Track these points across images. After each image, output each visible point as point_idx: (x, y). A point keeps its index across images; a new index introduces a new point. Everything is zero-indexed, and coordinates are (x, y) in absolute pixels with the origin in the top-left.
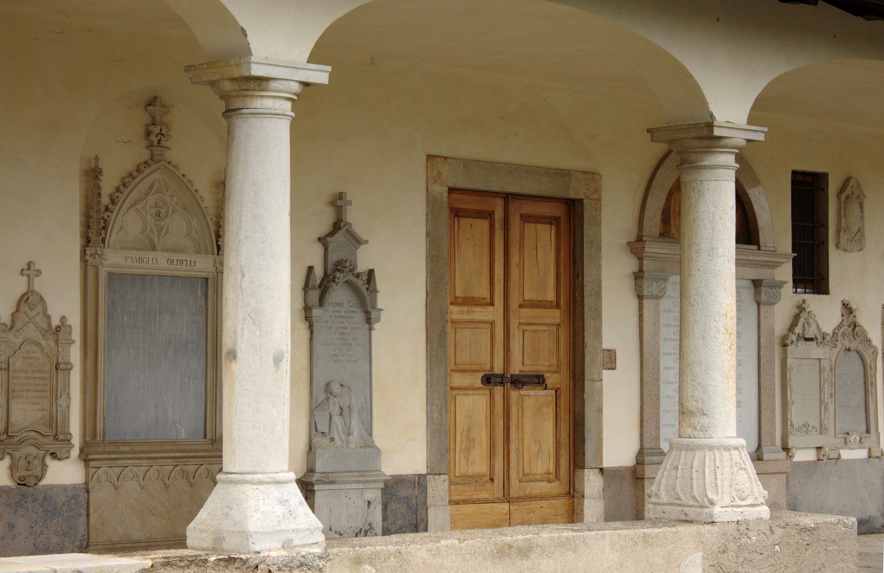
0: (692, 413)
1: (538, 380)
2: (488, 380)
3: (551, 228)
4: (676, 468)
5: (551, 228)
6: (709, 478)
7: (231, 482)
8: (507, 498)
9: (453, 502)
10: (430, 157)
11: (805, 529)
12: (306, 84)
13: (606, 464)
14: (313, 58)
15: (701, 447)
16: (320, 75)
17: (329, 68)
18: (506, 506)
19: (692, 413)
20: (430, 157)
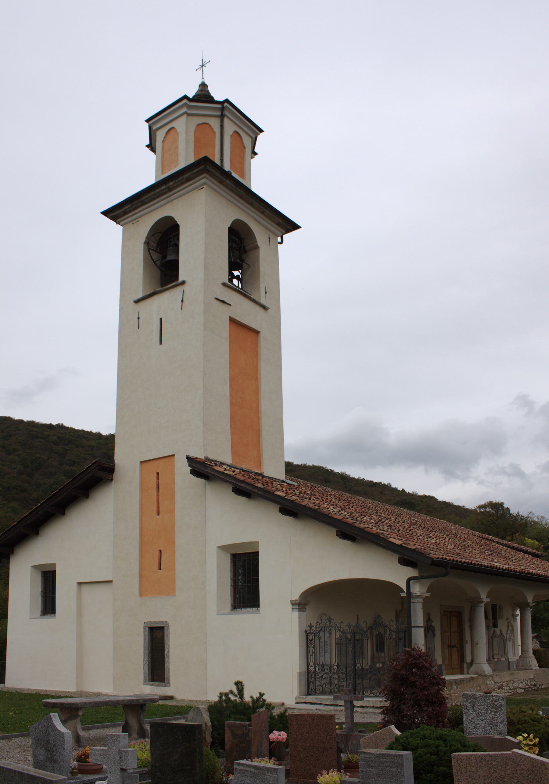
0: (525, 652)
1: (455, 646)
2: (448, 646)
3: (414, 602)
4: (523, 661)
5: (414, 602)
6: (530, 662)
7: (476, 664)
8: (452, 668)
9: (446, 669)
10: (440, 605)
11: (544, 671)
12: (426, 596)
13: (467, 662)
14: (427, 592)
15: (528, 657)
16: (428, 595)
17: (430, 594)
18: (451, 670)
19: (525, 652)
20: (440, 605)
